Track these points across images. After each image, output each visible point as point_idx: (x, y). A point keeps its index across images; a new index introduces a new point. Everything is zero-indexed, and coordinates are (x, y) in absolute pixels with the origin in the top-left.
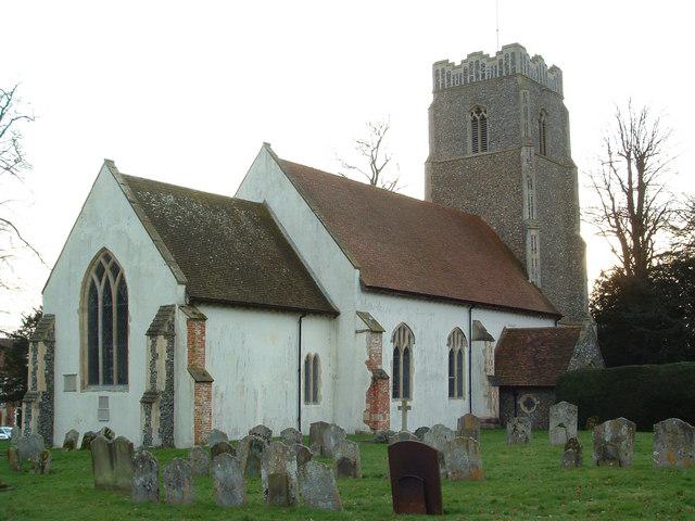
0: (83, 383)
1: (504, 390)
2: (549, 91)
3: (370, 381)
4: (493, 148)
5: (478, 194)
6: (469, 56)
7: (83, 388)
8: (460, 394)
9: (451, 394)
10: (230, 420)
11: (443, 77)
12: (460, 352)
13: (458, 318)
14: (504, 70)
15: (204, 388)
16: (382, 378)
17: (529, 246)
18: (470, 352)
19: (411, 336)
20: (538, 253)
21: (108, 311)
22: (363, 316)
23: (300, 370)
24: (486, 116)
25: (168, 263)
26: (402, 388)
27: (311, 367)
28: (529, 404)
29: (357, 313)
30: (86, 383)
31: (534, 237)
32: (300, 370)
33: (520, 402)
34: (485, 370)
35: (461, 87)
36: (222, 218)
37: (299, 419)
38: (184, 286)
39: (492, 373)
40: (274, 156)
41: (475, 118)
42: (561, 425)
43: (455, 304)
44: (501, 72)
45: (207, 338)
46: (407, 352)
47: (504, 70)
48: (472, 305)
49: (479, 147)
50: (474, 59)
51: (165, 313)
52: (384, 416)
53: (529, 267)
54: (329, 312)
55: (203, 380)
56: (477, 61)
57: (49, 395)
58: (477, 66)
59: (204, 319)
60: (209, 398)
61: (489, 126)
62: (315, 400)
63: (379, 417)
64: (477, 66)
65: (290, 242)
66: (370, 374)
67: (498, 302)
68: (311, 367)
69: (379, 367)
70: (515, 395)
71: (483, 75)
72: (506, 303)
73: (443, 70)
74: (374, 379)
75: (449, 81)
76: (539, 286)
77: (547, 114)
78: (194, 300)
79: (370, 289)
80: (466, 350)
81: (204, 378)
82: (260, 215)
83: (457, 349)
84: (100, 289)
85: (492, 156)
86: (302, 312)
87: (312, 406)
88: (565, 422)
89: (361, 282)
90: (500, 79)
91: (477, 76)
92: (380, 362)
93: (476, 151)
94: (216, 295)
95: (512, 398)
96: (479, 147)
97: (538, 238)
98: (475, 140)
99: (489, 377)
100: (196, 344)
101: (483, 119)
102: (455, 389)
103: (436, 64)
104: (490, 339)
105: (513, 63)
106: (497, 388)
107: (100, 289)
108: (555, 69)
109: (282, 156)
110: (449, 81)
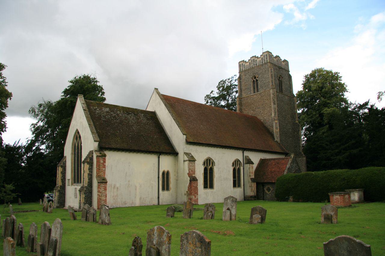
0: (72, 182)
1: (258, 184)
2: (282, 68)
3: (189, 181)
4: (261, 91)
5: (256, 109)
6: (251, 58)
7: (72, 184)
8: (239, 186)
9: (234, 186)
10: (122, 198)
11: (242, 67)
12: (239, 169)
13: (238, 155)
14: (263, 61)
15: (102, 185)
16: (194, 180)
17: (274, 127)
18: (244, 169)
19: (213, 163)
20: (278, 129)
21: (78, 153)
22: (186, 154)
23: (159, 177)
24: (258, 79)
25: (93, 133)
26: (209, 183)
27: (166, 176)
28: (269, 190)
29: (185, 153)
30: (73, 182)
31: (276, 123)
32: (159, 177)
33: (265, 189)
34: (250, 176)
35: (249, 69)
36: (131, 118)
37: (159, 198)
38: (98, 143)
39: (253, 177)
40: (158, 93)
41: (254, 80)
42: (228, 209)
43: (235, 149)
44: (262, 62)
45: (106, 164)
46: (212, 170)
47: (263, 61)
48: (244, 149)
49: (256, 91)
50: (253, 59)
51: (91, 153)
52: (195, 197)
53: (275, 135)
54: (173, 152)
55: (103, 181)
56: (254, 59)
57: (63, 187)
58: (254, 61)
59: (105, 156)
60: (105, 189)
61: (259, 82)
62: (168, 189)
63: (193, 197)
64: (254, 61)
65: (162, 126)
66: (189, 179)
67: (257, 148)
68: (166, 176)
69: (193, 175)
70: (263, 186)
71: (256, 64)
72: (262, 149)
73: (242, 64)
74: (190, 181)
75: (244, 68)
76: (279, 142)
77: (282, 78)
78: (103, 148)
79: (188, 143)
80: (242, 168)
81: (104, 181)
82: (153, 116)
83: (237, 168)
84: (77, 145)
85: (260, 94)
86: (159, 153)
87: (166, 192)
88: (230, 207)
89: (186, 140)
90: (262, 65)
91: (254, 65)
92: (194, 173)
93: (254, 92)
94: (113, 146)
95: (262, 187)
96: (256, 91)
97: (278, 123)
98: (254, 88)
99: (251, 179)
100: (102, 167)
101: (257, 80)
102: (236, 183)
103: (239, 62)
104: (252, 163)
105: (267, 59)
106: (255, 184)
107: (77, 145)
108: (285, 61)
109: (162, 92)
110: (244, 68)
